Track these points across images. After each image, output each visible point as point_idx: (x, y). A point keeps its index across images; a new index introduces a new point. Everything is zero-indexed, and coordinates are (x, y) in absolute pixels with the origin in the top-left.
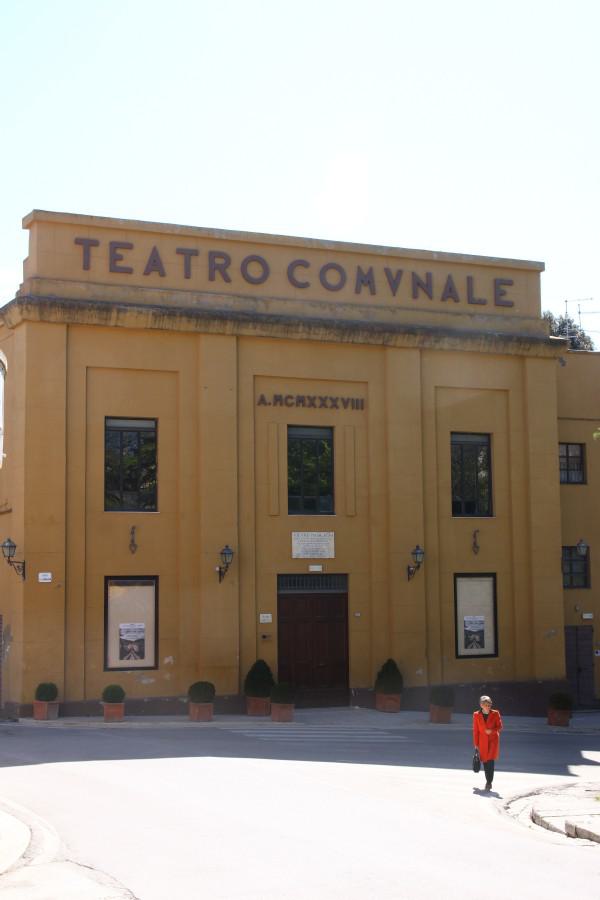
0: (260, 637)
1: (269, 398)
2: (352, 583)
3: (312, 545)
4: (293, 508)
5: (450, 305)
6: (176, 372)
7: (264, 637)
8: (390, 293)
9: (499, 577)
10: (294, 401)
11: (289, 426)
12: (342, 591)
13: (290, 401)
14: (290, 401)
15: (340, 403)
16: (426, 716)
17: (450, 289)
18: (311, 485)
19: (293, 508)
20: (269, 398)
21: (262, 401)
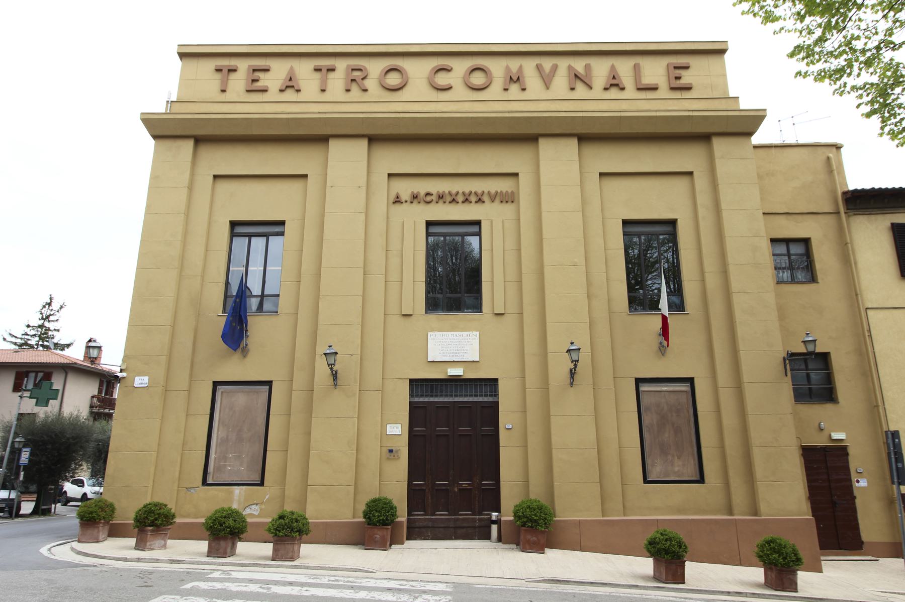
0: (385, 450)
1: (405, 196)
2: (503, 388)
3: (455, 346)
4: (432, 305)
5: (614, 93)
6: (516, 175)
7: (391, 451)
8: (543, 87)
9: (696, 381)
10: (434, 198)
11: (626, 223)
12: (491, 399)
13: (429, 198)
14: (429, 198)
15: (485, 198)
16: (132, 541)
17: (576, 75)
18: (454, 283)
19: (432, 305)
20: (405, 196)
21: (398, 201)
